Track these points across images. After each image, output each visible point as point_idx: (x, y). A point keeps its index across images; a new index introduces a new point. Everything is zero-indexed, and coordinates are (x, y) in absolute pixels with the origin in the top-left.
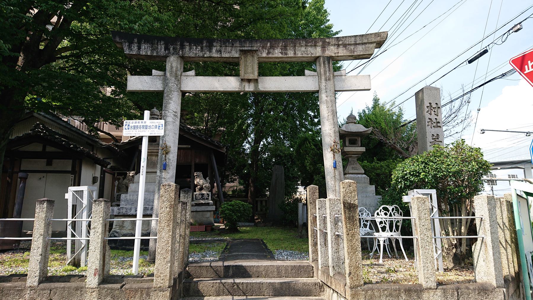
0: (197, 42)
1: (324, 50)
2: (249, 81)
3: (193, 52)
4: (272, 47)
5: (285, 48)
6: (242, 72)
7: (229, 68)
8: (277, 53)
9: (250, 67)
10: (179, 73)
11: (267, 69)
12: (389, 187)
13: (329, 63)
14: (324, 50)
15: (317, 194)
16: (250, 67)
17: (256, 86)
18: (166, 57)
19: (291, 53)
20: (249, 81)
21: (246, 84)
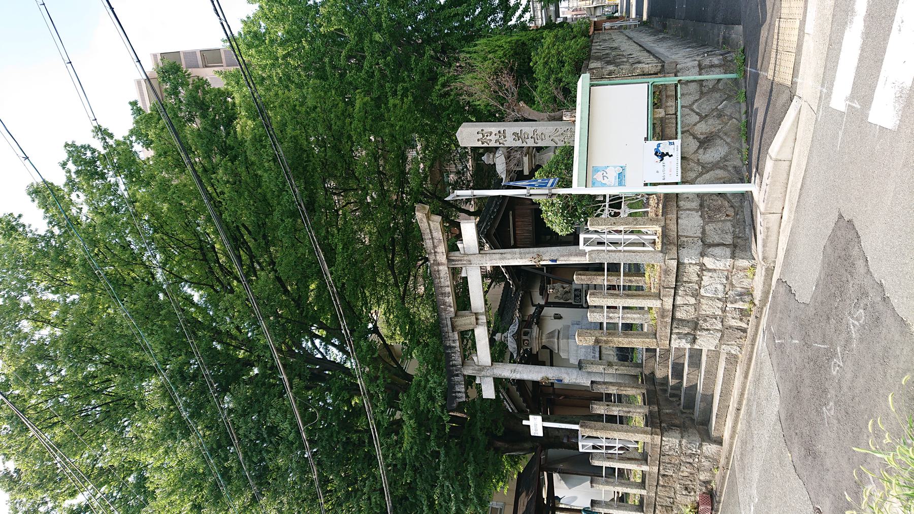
0: (449, 357)
1: (442, 264)
2: (477, 319)
3: (457, 359)
4: (444, 304)
5: (443, 294)
6: (471, 327)
7: (468, 338)
8: (450, 300)
9: (465, 321)
10: (477, 368)
11: (463, 301)
12: (229, 94)
13: (453, 260)
14: (442, 264)
15: (572, 248)
16: (465, 321)
17: (482, 314)
18: (464, 376)
19: (448, 290)
20: (477, 319)
21: (480, 321)
